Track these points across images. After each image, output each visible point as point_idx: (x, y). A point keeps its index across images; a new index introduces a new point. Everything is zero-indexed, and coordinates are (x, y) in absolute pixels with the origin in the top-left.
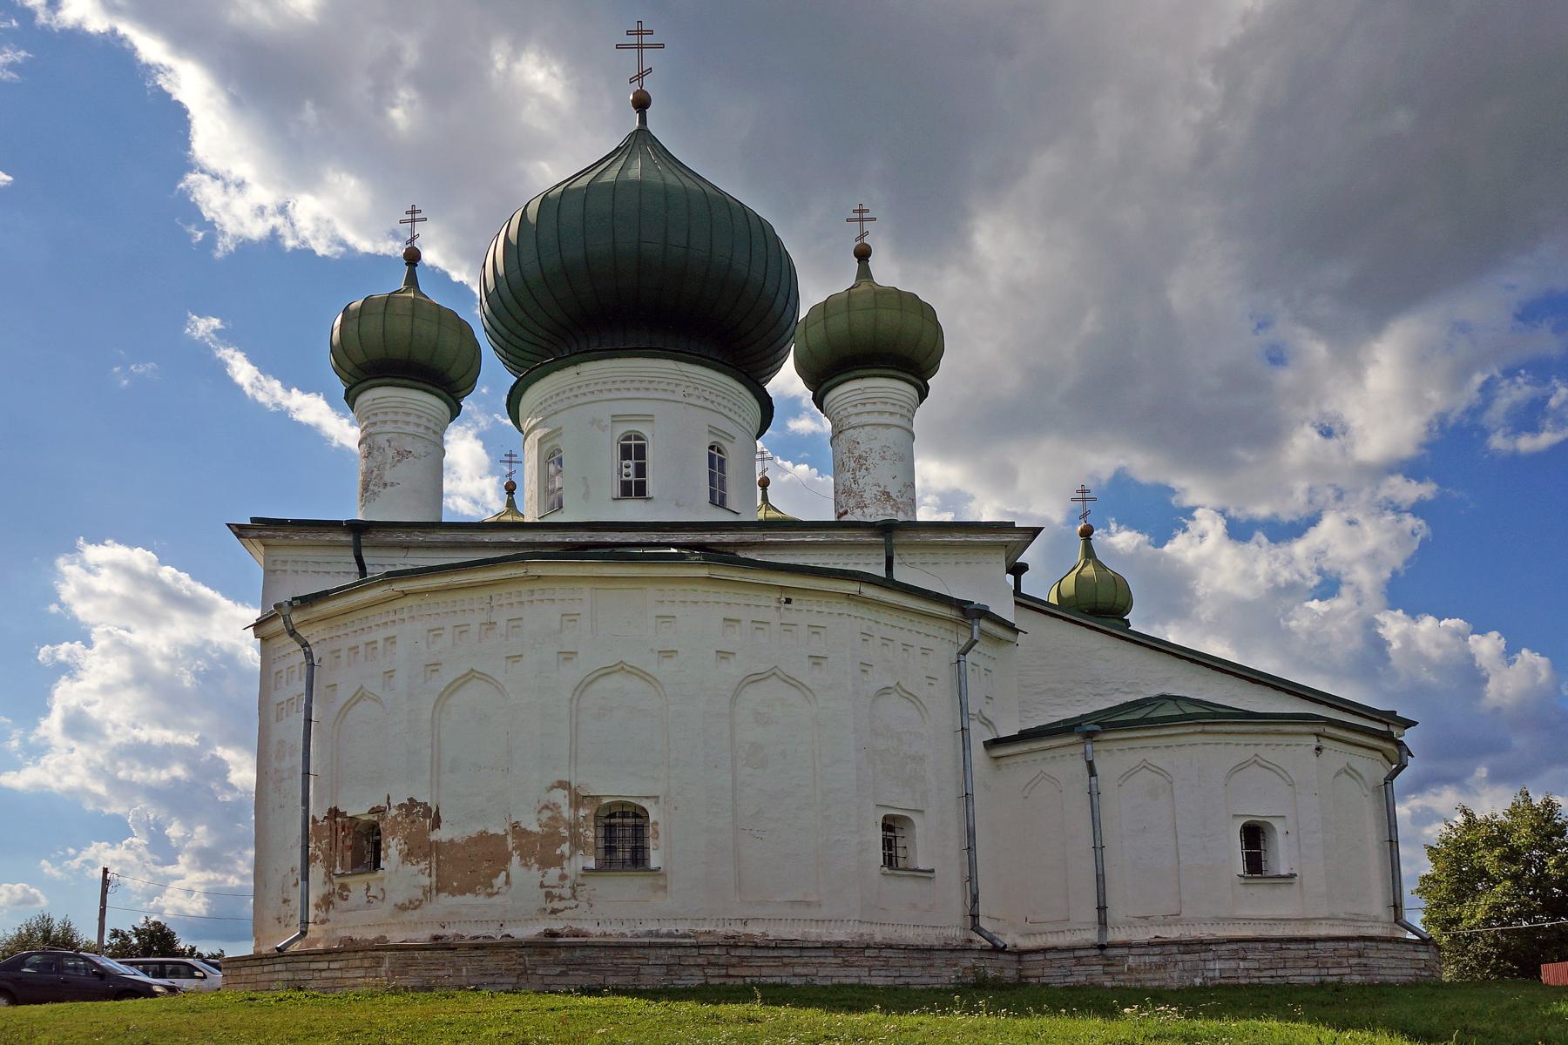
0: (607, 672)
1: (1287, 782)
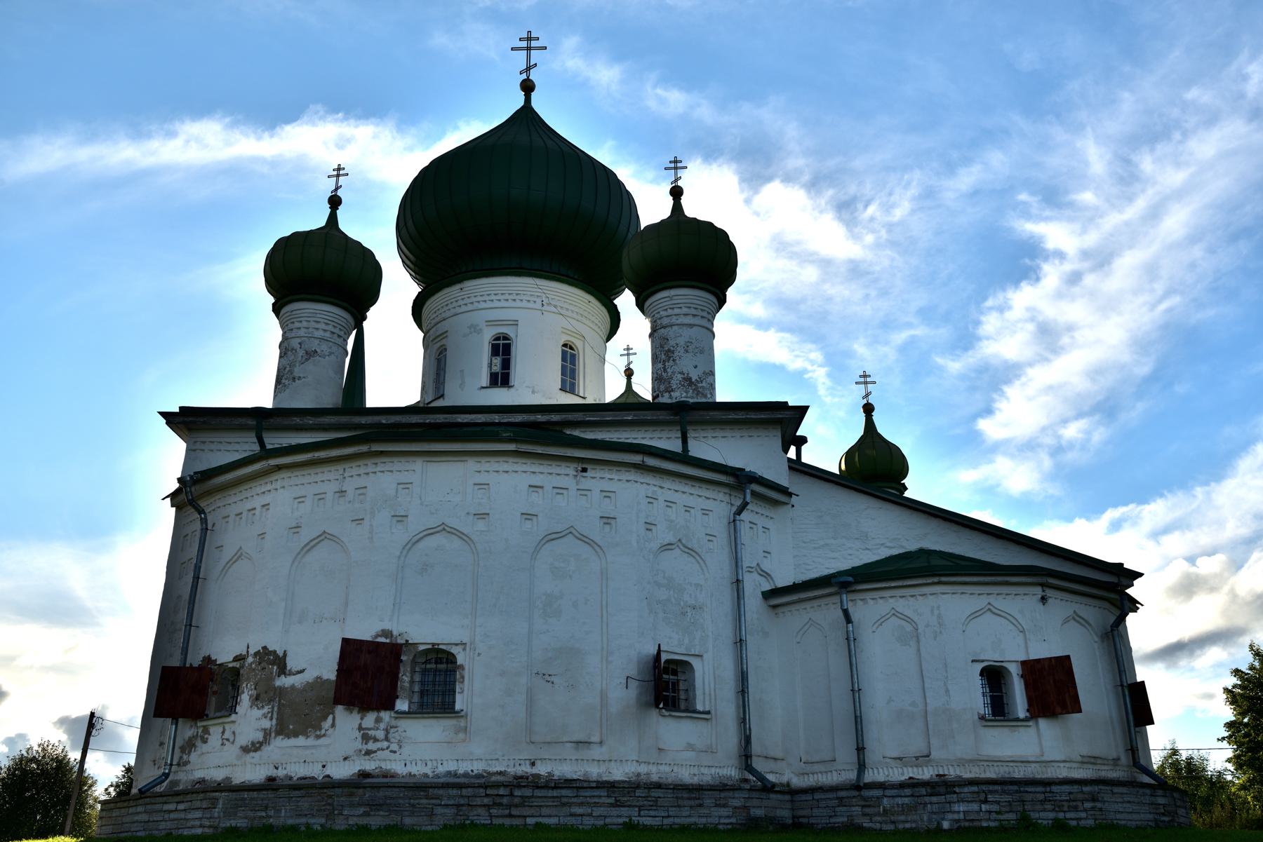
0: (430, 532)
1: (1019, 629)
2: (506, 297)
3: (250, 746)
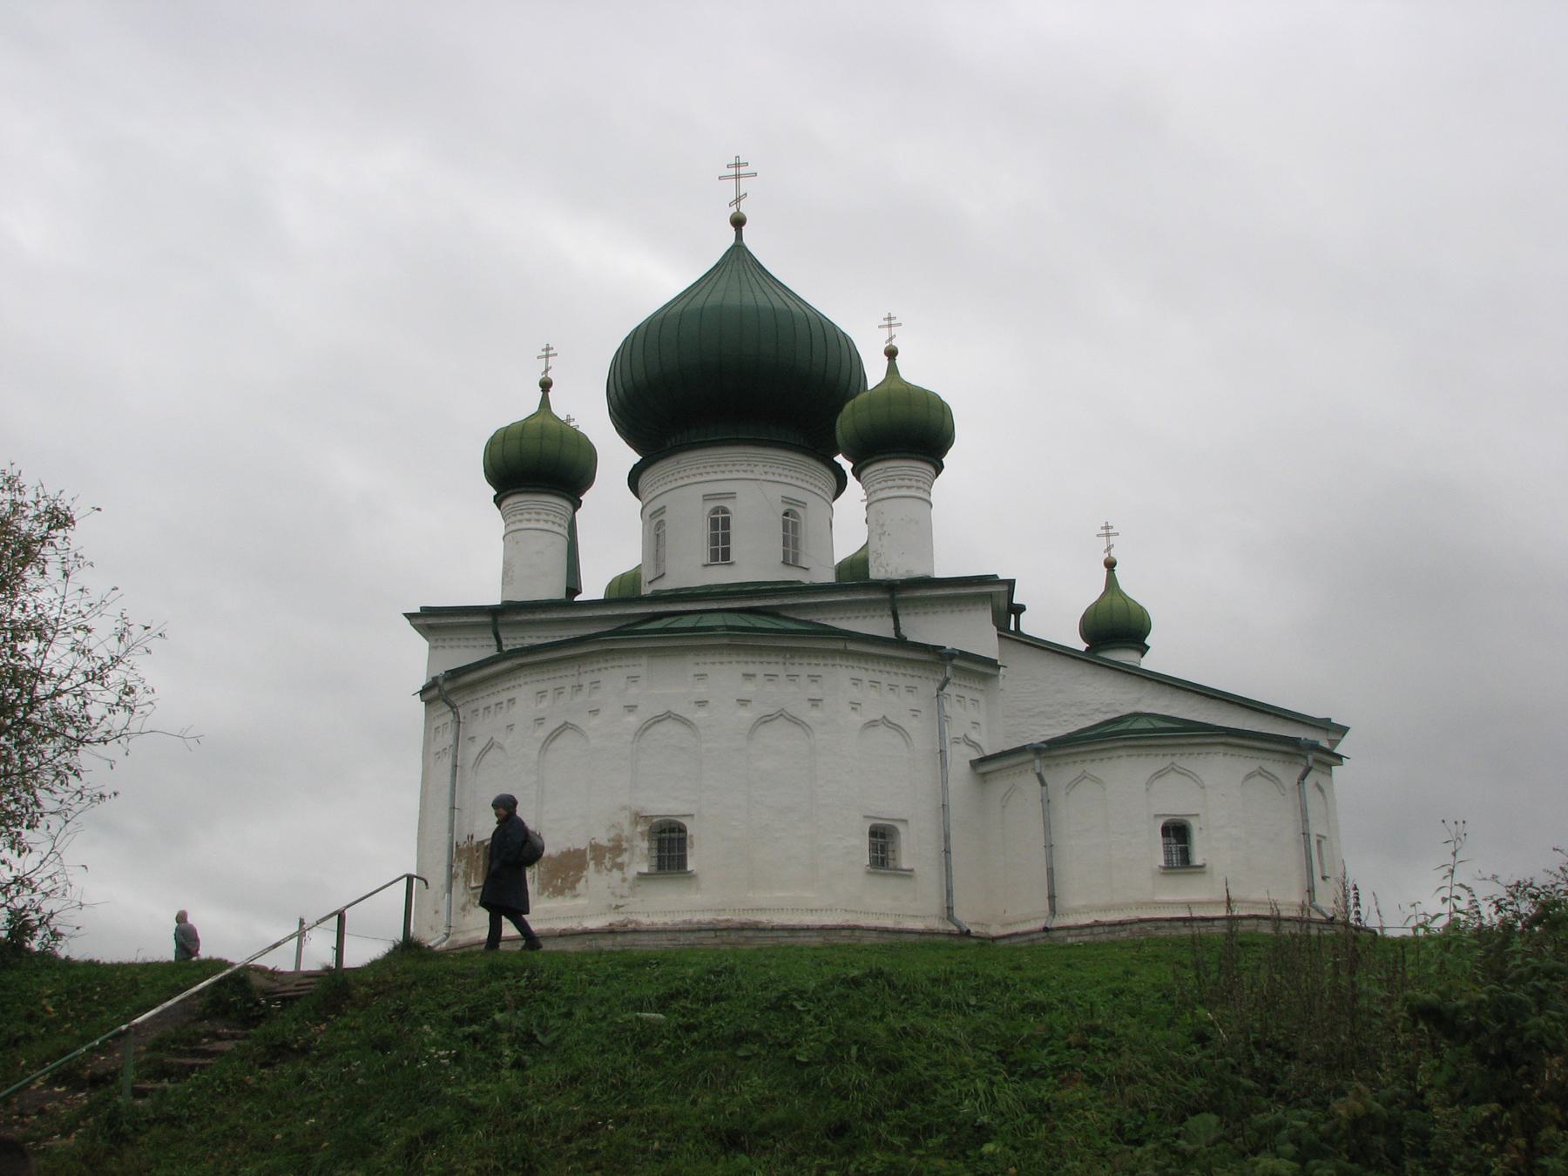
0: (658, 720)
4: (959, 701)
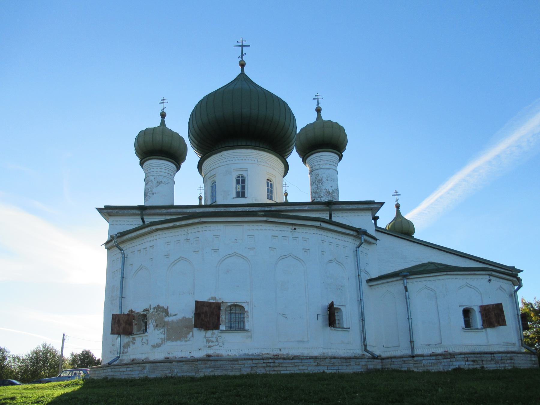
0: (230, 256)
1: (479, 293)
2: (242, 158)
3: (156, 345)
4: (366, 255)
